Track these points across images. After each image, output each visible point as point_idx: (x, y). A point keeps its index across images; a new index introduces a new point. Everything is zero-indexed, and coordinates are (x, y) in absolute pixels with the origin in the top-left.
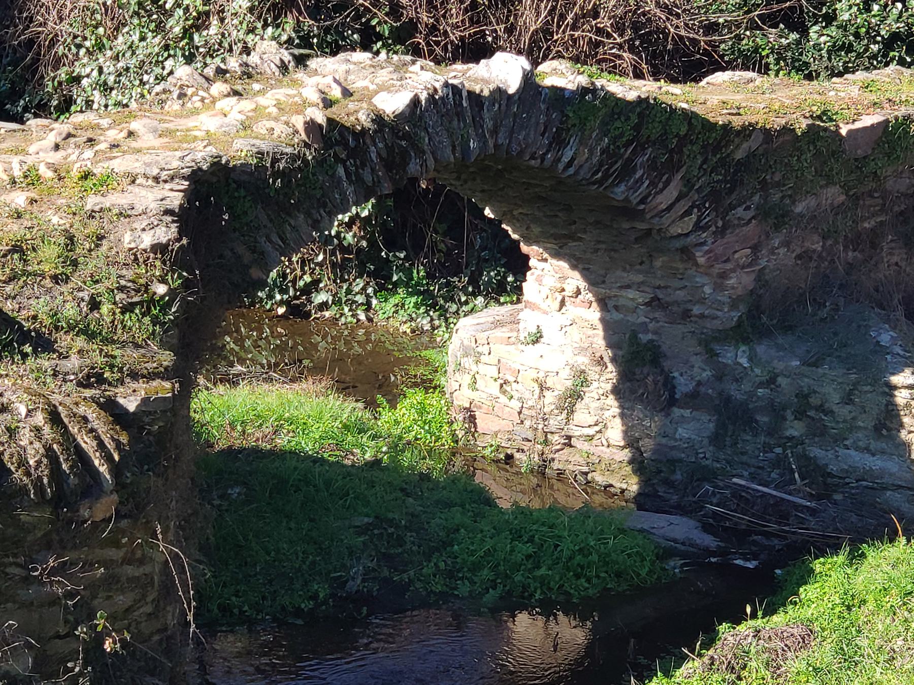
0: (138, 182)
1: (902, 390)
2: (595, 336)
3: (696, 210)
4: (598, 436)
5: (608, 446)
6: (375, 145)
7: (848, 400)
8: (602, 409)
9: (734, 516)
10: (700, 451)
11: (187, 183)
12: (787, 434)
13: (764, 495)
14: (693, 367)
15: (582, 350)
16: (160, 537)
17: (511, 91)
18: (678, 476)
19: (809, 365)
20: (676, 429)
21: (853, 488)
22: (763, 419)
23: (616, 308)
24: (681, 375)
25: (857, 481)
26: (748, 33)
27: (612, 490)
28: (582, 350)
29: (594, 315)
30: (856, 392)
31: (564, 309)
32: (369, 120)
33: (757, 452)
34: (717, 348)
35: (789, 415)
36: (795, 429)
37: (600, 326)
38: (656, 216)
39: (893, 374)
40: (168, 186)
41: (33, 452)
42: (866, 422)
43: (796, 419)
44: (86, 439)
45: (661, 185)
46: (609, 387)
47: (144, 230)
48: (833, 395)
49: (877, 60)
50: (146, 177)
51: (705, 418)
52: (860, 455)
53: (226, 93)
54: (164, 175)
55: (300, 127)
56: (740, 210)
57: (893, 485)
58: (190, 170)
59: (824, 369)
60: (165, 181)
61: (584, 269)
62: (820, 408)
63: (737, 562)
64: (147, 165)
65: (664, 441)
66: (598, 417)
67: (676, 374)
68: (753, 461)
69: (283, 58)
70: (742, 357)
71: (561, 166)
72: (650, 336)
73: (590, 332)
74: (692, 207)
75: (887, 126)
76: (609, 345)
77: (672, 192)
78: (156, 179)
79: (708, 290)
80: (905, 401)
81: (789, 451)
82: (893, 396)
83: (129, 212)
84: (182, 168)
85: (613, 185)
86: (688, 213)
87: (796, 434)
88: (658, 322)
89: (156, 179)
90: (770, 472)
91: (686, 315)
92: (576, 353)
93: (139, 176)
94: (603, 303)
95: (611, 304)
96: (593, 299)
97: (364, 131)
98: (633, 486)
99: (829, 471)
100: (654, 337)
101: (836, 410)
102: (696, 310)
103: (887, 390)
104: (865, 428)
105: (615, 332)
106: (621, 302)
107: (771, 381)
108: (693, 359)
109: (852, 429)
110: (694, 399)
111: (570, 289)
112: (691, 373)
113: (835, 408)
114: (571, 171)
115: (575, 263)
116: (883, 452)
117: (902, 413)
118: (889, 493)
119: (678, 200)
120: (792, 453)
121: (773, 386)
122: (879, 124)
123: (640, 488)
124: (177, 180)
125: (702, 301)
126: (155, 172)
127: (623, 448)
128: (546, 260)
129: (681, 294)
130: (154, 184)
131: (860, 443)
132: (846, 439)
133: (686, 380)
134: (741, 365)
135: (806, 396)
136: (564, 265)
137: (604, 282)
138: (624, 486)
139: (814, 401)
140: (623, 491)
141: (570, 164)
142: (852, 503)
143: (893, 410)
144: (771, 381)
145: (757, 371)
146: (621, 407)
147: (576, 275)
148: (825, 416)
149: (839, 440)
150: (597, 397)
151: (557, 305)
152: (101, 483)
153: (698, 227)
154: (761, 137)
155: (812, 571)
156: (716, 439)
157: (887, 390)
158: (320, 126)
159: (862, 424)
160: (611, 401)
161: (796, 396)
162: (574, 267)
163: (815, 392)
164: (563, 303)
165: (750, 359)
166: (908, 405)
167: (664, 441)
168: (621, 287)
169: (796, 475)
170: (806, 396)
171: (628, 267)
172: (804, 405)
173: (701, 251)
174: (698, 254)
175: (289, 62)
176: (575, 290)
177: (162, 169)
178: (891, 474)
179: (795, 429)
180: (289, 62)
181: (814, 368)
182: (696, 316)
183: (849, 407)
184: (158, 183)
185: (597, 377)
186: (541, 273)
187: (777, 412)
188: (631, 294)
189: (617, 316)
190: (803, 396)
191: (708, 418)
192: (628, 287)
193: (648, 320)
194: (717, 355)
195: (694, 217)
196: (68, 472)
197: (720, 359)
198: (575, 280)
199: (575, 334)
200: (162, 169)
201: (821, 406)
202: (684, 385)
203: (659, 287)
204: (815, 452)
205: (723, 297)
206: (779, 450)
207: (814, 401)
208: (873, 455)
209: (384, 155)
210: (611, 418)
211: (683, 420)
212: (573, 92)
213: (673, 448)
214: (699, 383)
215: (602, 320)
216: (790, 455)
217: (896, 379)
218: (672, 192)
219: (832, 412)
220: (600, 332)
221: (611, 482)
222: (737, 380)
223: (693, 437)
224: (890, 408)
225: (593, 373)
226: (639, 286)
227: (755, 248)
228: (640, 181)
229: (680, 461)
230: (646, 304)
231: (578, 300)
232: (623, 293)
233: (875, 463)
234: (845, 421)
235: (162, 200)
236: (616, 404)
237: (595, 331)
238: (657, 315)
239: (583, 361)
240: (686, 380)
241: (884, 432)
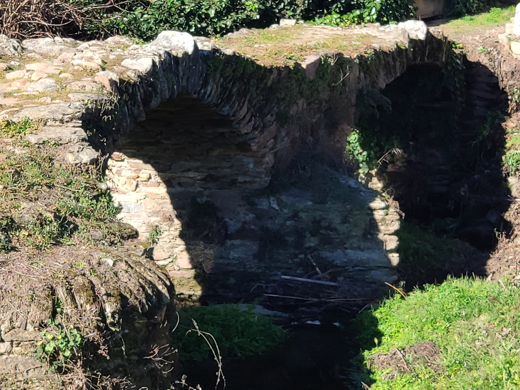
0: (48, 124)
1: (378, 211)
2: (164, 203)
3: (253, 118)
4: (171, 265)
5: (179, 270)
6: (139, 91)
7: (345, 221)
8: (172, 248)
9: (297, 296)
10: (247, 264)
11: (81, 122)
12: (307, 245)
13: (303, 283)
14: (239, 213)
15: (156, 213)
16: (197, 327)
17: (190, 53)
18: (232, 281)
19: (319, 203)
20: (229, 253)
21: (351, 272)
22: (291, 239)
23: (180, 184)
24: (231, 219)
25: (353, 267)
26: (105, 15)
27: (182, 296)
28: (156, 213)
29: (162, 190)
30: (350, 216)
31: (138, 190)
32: (136, 76)
33: (287, 259)
34: (257, 201)
35: (308, 235)
36: (312, 242)
37: (167, 197)
38: (237, 123)
39: (371, 202)
40: (70, 124)
41: (133, 285)
42: (357, 232)
43: (312, 236)
44: (150, 274)
45: (241, 104)
46: (177, 233)
47: (78, 152)
48: (336, 220)
49: (182, 27)
50: (55, 120)
51: (248, 243)
52: (355, 252)
53: (5, 68)
54: (66, 118)
55: (107, 84)
56: (269, 116)
57: (376, 267)
58: (81, 113)
59: (329, 204)
60: (67, 122)
61: (155, 163)
62: (329, 228)
63: (309, 322)
64: (53, 112)
65: (221, 261)
66: (170, 253)
67: (227, 220)
68: (285, 265)
69: (14, 44)
70: (274, 203)
71: (206, 97)
72: (205, 199)
73: (161, 201)
74: (251, 117)
75: (321, 62)
76: (175, 208)
77: (245, 109)
78: (62, 121)
79: (251, 166)
80: (381, 217)
81: (309, 256)
82: (373, 215)
83: (60, 142)
84: (76, 113)
85: (224, 106)
86: (250, 121)
87: (313, 245)
88: (211, 189)
89: (62, 121)
90: (297, 270)
91: (233, 183)
92: (149, 215)
93: (49, 120)
94: (168, 183)
95: (174, 182)
96: (161, 181)
97: (135, 83)
98: (198, 291)
99: (335, 264)
100: (209, 199)
101: (338, 228)
102: (241, 179)
103: (369, 212)
104: (356, 236)
105: (177, 200)
106: (183, 180)
107: (295, 216)
108: (239, 209)
109: (348, 238)
110: (243, 233)
111: (144, 175)
112: (239, 216)
113: (338, 227)
114: (210, 99)
115: (148, 160)
116: (369, 249)
117: (380, 224)
118: (373, 272)
119: (247, 113)
120: (311, 256)
121: (296, 218)
122: (317, 60)
123: (203, 292)
124: (75, 121)
125: (245, 174)
126: (60, 117)
127: (192, 269)
128: (123, 161)
129: (228, 171)
130: (61, 124)
131: (354, 245)
132: (345, 244)
133: (235, 222)
134: (274, 208)
135: (319, 222)
136: (139, 162)
137: (170, 169)
138: (192, 293)
139: (324, 224)
140: (190, 296)
141: (209, 96)
142: (350, 281)
143: (374, 223)
144: (295, 216)
145: (286, 211)
146: (186, 244)
147: (149, 166)
148: (331, 231)
149: (342, 244)
150: (168, 241)
151: (134, 187)
152: (162, 299)
153: (254, 128)
154: (277, 72)
155: (376, 319)
156: (259, 256)
157: (369, 212)
158: (115, 82)
159: (354, 234)
160: (179, 241)
161: (313, 222)
162: (146, 162)
163: (323, 218)
164: (137, 186)
165: (279, 205)
166: (383, 219)
167: (221, 261)
168: (184, 171)
169: (317, 269)
170: (319, 222)
171: (188, 158)
172: (317, 227)
173: (254, 143)
174: (252, 144)
175: (18, 46)
176: (148, 176)
177: (64, 115)
178: (374, 261)
179: (312, 242)
180: (18, 46)
181: (323, 205)
182: (241, 183)
183: (347, 225)
184: (63, 123)
185: (167, 228)
186: (119, 169)
187: (299, 234)
188: (191, 174)
189: (179, 189)
190: (317, 222)
191: (252, 243)
192: (189, 170)
193: (202, 189)
194: (256, 205)
195: (253, 122)
196: (152, 294)
197: (259, 207)
198: (147, 170)
199: (150, 205)
200: (64, 115)
201: (329, 226)
202: (233, 226)
203: (211, 169)
204: (326, 254)
205: (261, 169)
206: (302, 256)
207: (324, 224)
208: (362, 251)
209: (143, 97)
210: (179, 252)
211: (233, 246)
212: (209, 52)
213: (228, 264)
214: (244, 223)
215: (169, 193)
216: (310, 258)
217: (373, 205)
218: (245, 109)
219: (335, 229)
220: (168, 201)
221: (182, 292)
222: (272, 218)
223: (242, 256)
224: (373, 222)
225: (164, 226)
226: (197, 170)
227: (275, 138)
228: (234, 103)
229: (233, 271)
230: (202, 180)
231: (149, 183)
232: (185, 174)
233: (364, 256)
234: (344, 233)
235: (75, 133)
236: (183, 243)
237: (164, 200)
238: (210, 185)
239: (155, 220)
240: (235, 222)
241: (369, 236)
